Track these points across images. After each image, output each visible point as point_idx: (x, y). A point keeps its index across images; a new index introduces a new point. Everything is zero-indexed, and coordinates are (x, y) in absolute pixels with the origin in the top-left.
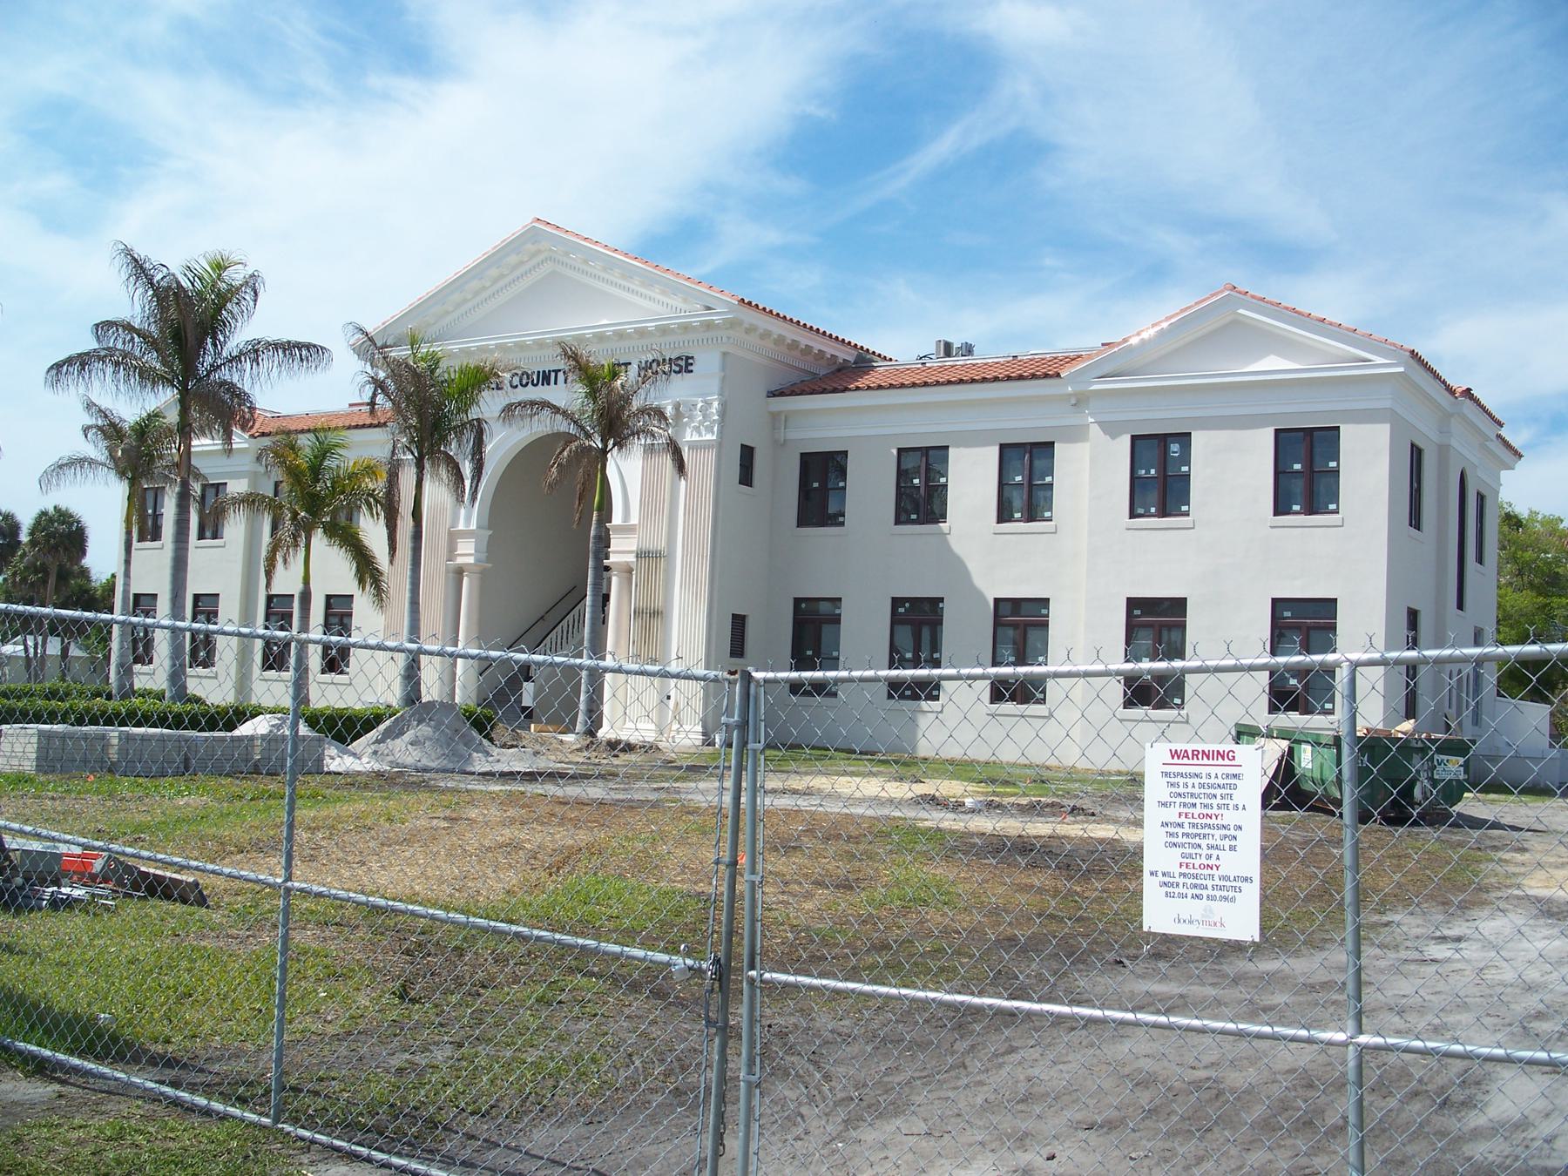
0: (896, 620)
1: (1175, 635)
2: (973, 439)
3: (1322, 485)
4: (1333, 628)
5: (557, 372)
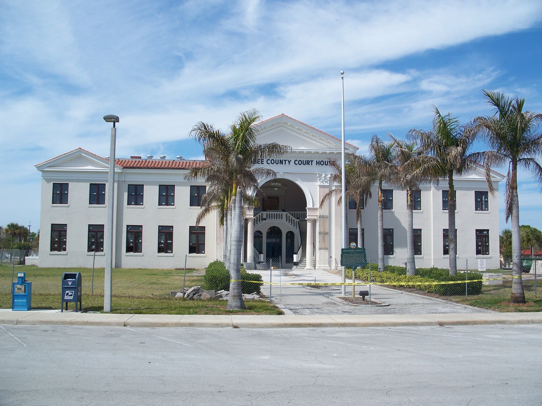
0: (191, 233)
1: (64, 233)
2: (151, 183)
3: (170, 199)
4: (204, 233)
5: (285, 161)
